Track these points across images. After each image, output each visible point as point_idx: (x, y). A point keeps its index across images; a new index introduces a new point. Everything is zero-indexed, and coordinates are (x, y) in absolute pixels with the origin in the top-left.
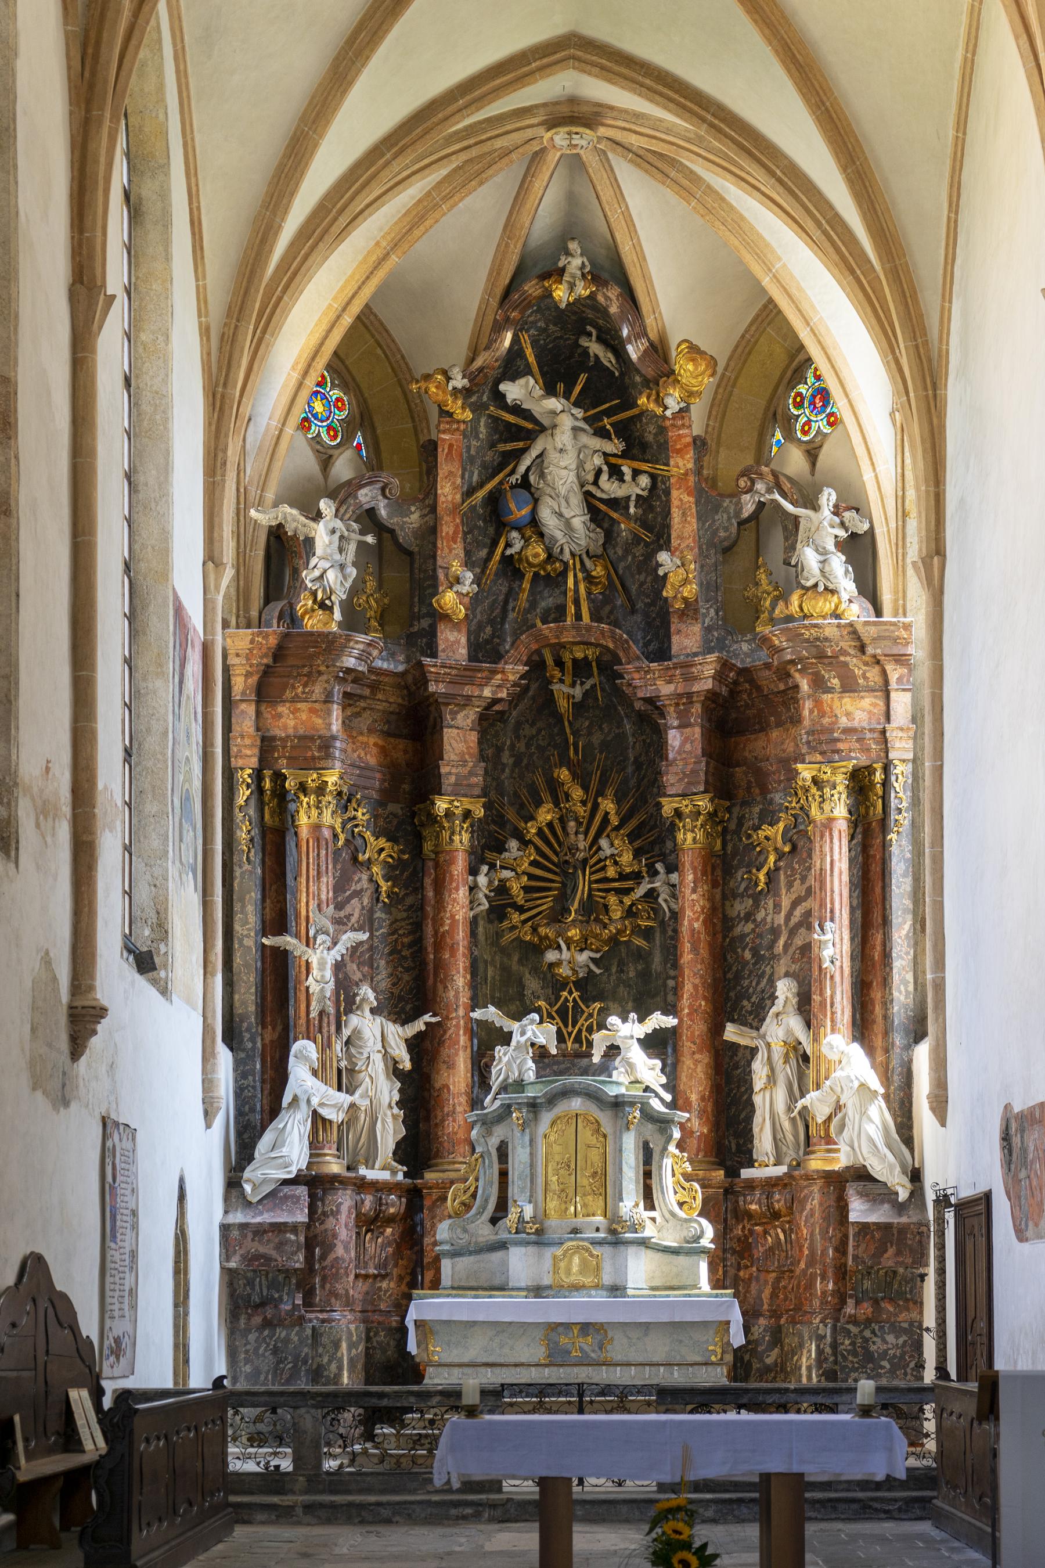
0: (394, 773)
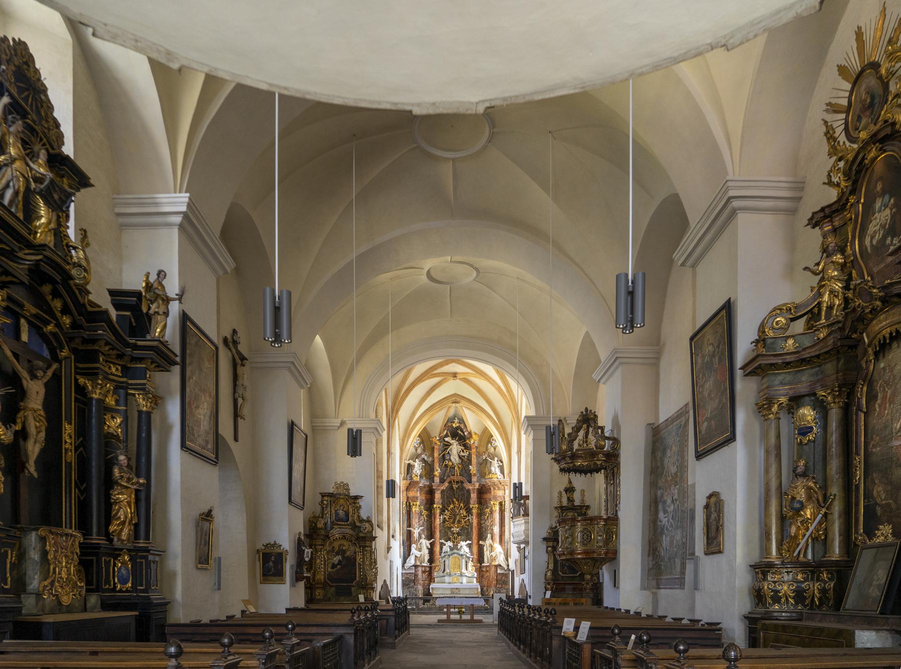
0: (427, 500)
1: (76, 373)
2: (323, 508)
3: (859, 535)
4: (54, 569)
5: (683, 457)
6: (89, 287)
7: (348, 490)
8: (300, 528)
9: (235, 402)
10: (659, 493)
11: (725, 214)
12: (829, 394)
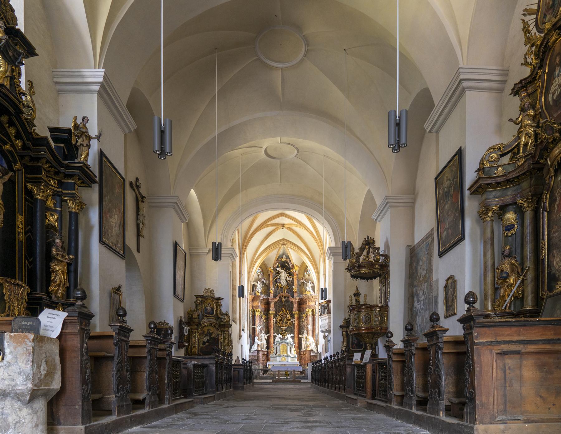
0: (265, 308)
1: (26, 181)
2: (197, 305)
3: (545, 293)
4: (9, 307)
5: (430, 264)
6: (35, 122)
7: (213, 294)
8: (181, 313)
9: (138, 225)
10: (414, 289)
11: (457, 92)
12: (525, 202)
